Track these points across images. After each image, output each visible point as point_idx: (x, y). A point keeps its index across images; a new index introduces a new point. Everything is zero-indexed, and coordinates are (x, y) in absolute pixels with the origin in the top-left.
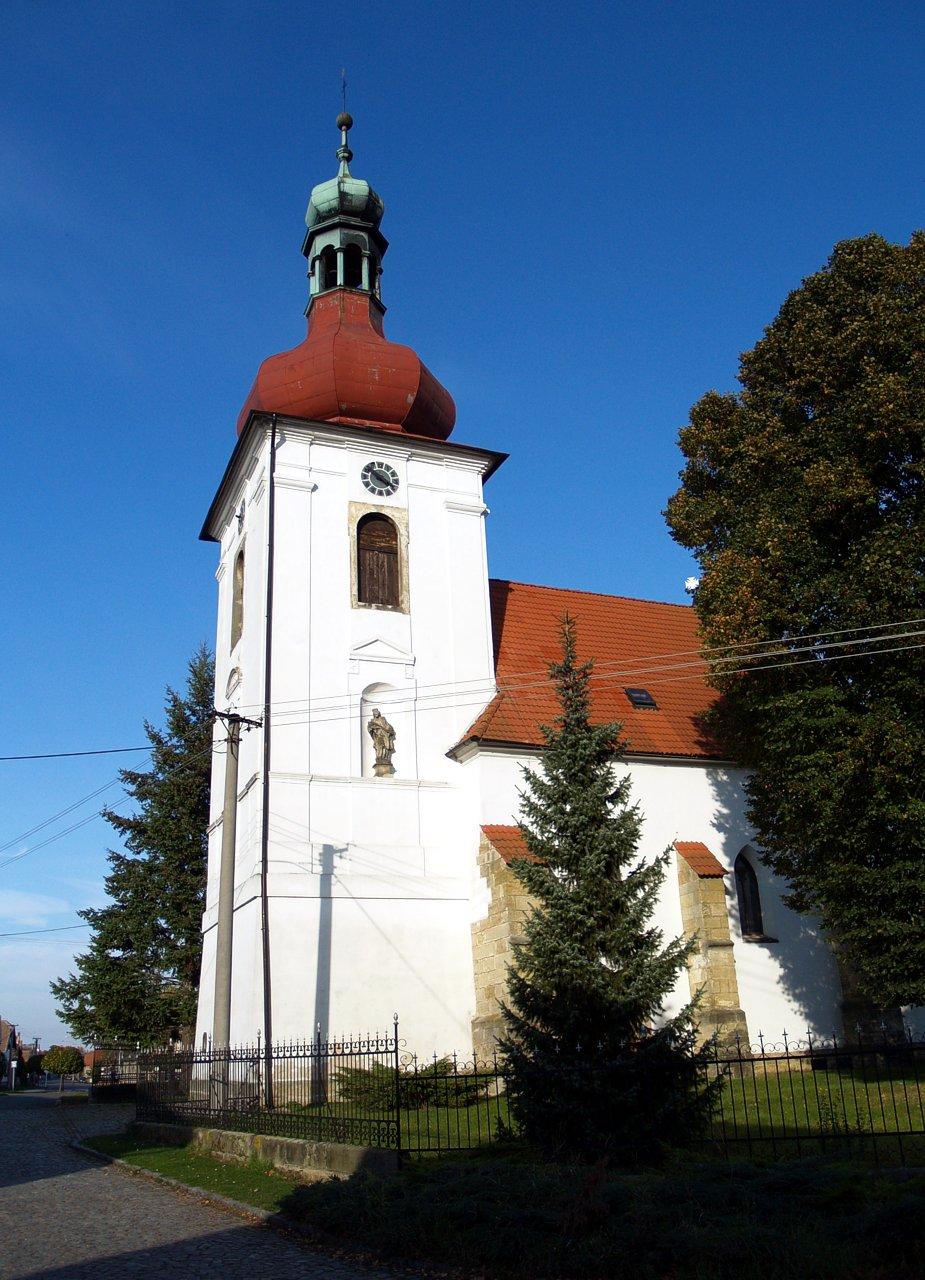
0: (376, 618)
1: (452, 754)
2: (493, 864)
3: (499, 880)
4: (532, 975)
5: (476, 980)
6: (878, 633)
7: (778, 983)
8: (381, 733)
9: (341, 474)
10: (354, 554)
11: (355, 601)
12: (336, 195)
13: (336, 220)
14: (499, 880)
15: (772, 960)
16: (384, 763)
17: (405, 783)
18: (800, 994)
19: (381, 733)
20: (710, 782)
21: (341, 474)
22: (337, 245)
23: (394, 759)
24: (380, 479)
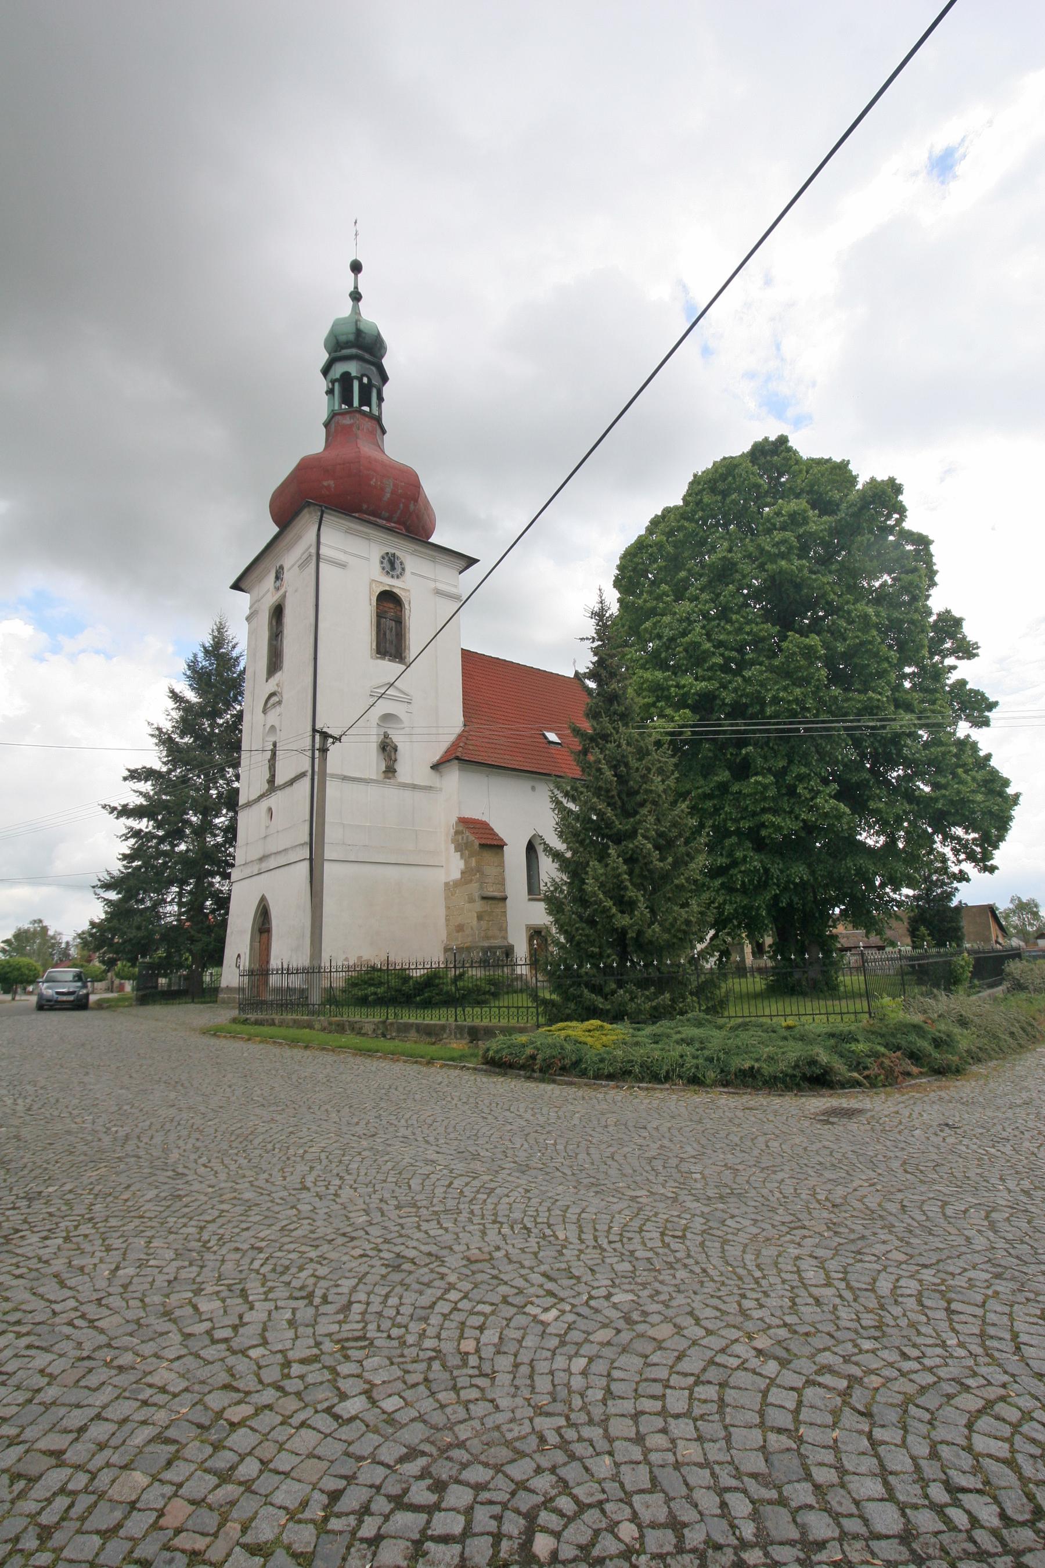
0: (389, 668)
1: (435, 767)
2: (466, 844)
3: (471, 856)
4: (710, 754)
5: (447, 920)
6: (760, 731)
7: (1017, 796)
8: (387, 749)
9: (275, 745)
10: (374, 620)
11: (374, 652)
12: (354, 330)
13: (353, 351)
14: (471, 856)
15: (1005, 773)
16: (390, 771)
17: (405, 786)
18: (998, 829)
19: (387, 749)
20: (557, 865)
21: (275, 745)
22: (354, 374)
23: (399, 767)
24: (391, 564)
